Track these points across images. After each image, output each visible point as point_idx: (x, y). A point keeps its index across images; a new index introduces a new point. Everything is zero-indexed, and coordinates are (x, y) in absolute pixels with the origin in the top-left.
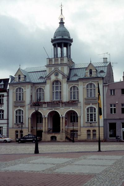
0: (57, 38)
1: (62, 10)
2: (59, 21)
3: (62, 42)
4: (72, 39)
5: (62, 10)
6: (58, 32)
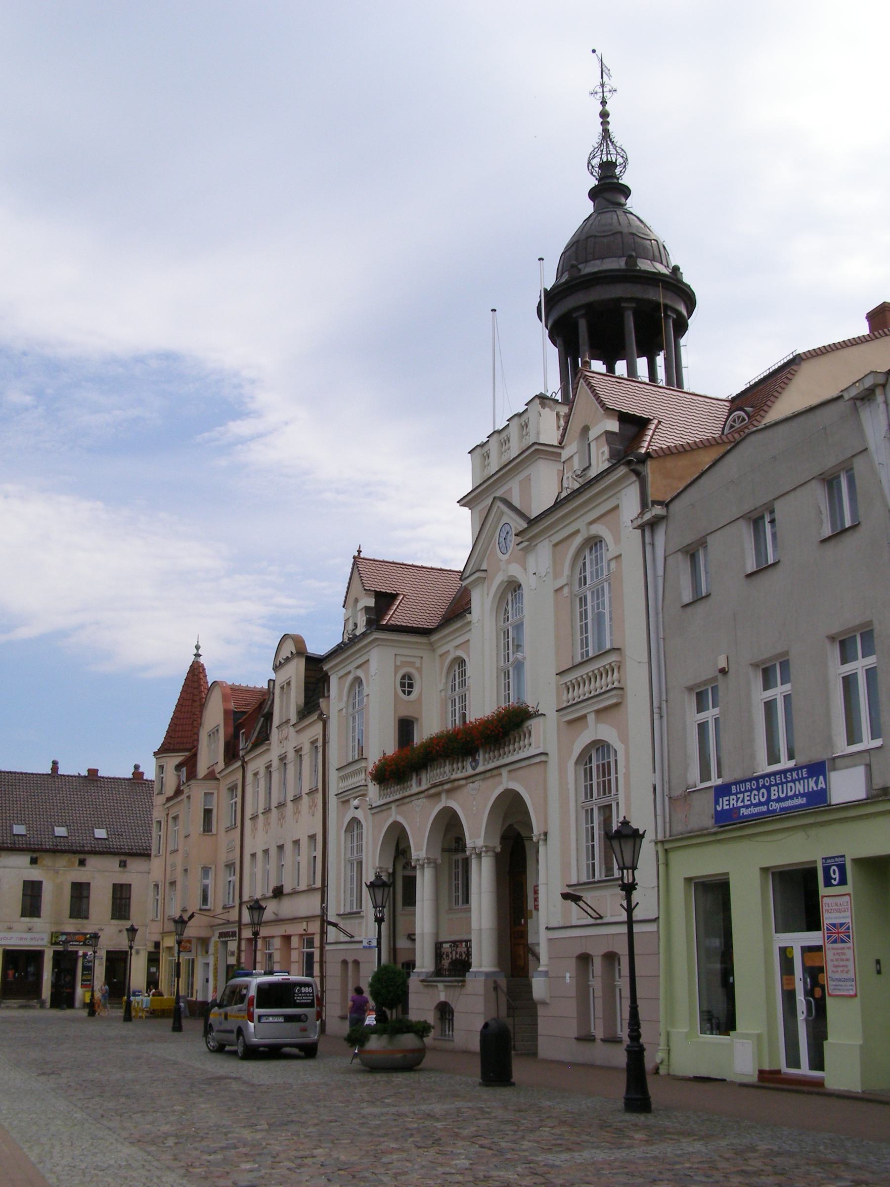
0: (589, 269)
1: (604, 115)
2: (593, 182)
3: (619, 300)
4: (676, 269)
5: (604, 115)
6: (580, 249)
